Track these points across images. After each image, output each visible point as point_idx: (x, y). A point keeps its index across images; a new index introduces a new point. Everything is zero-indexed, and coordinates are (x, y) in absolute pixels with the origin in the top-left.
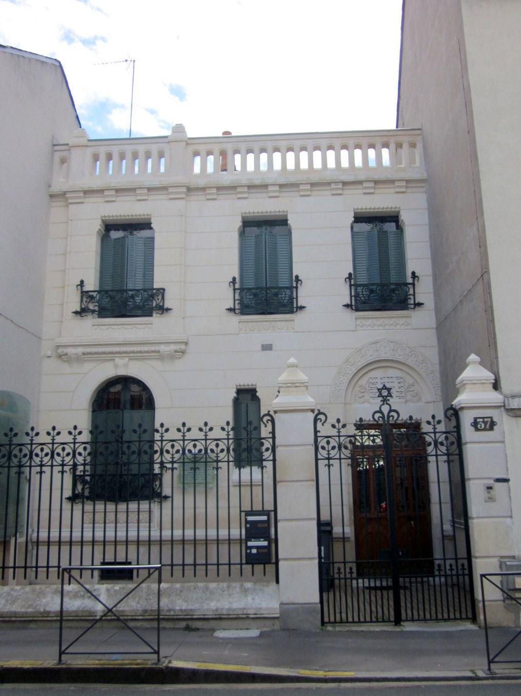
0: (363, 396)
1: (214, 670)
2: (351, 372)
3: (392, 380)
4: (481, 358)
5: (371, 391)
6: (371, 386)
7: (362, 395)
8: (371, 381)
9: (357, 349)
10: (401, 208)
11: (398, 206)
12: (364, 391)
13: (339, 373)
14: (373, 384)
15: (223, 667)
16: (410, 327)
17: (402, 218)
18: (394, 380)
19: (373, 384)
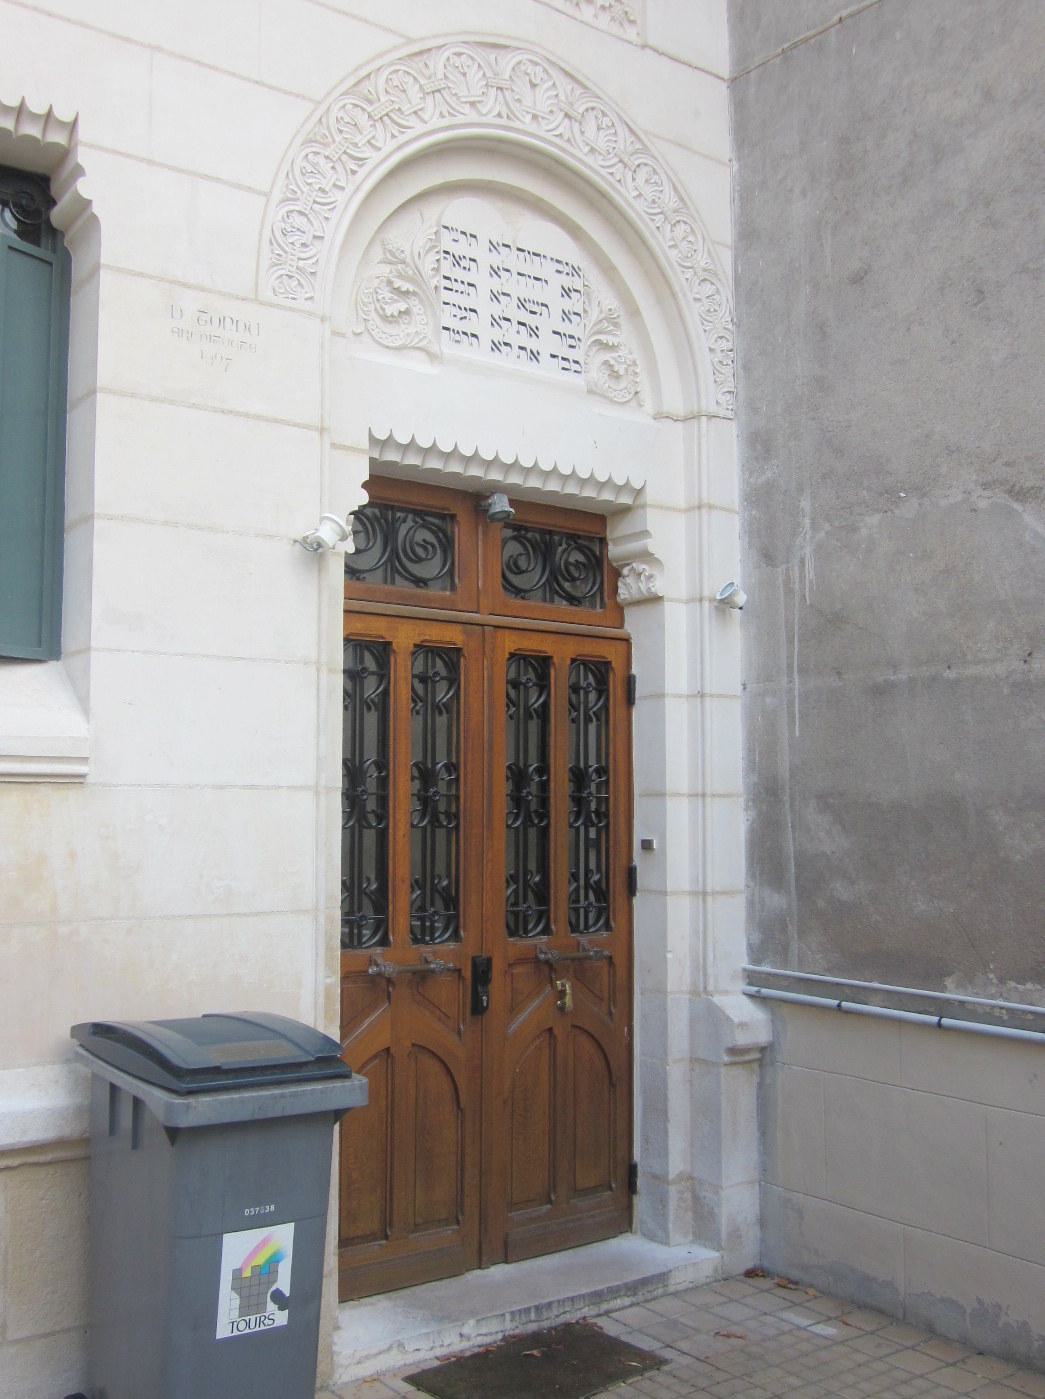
0: (407, 312)
1: (344, 729)
2: (374, 157)
3: (534, 267)
4: (616, 583)
5: (446, 296)
6: (447, 267)
7: (403, 307)
8: (446, 242)
9: (410, 41)
10: (83, 133)
11: (64, 114)
12: (405, 286)
13: (309, 141)
14: (457, 262)
15: (404, 692)
16: (631, 33)
17: (84, 188)
18: (547, 270)
19: (457, 262)
